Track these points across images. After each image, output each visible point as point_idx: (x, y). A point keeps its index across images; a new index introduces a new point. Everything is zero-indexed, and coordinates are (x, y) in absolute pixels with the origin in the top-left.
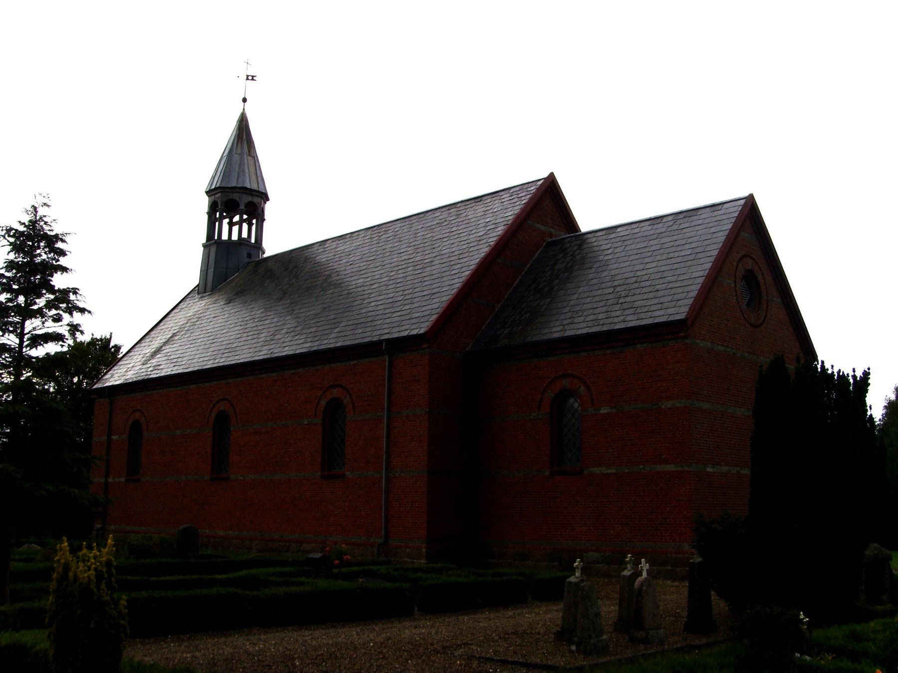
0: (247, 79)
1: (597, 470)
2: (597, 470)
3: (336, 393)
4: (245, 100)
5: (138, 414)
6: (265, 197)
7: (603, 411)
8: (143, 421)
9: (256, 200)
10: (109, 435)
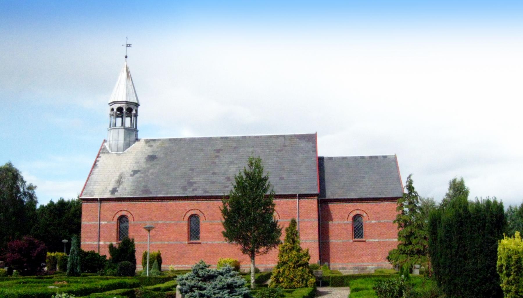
0: (127, 46)
1: (371, 240)
2: (371, 240)
4: (126, 57)
7: (373, 222)
9: (132, 106)
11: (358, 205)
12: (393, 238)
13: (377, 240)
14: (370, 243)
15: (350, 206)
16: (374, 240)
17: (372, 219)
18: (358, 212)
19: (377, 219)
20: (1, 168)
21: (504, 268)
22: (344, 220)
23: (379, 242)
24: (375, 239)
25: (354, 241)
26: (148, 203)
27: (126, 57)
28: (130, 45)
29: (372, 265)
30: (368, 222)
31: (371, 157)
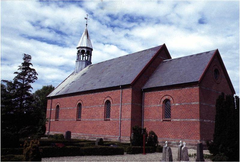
1: (175, 120)
2: (175, 120)
3: (108, 99)
5: (58, 103)
6: (92, 50)
7: (177, 104)
8: (60, 105)
9: (90, 50)
10: (51, 109)
11: (167, 92)
12: (190, 118)
13: (179, 120)
14: (174, 122)
15: (162, 93)
16: (177, 120)
17: (176, 103)
18: (167, 97)
19: (179, 102)
20: (22, 107)
21: (132, 20)
22: (158, 104)
23: (180, 122)
24: (177, 119)
25: (163, 121)
26: (102, 87)
27: (87, 25)
28: (85, 19)
29: (175, 141)
30: (173, 105)
31: (197, 55)
